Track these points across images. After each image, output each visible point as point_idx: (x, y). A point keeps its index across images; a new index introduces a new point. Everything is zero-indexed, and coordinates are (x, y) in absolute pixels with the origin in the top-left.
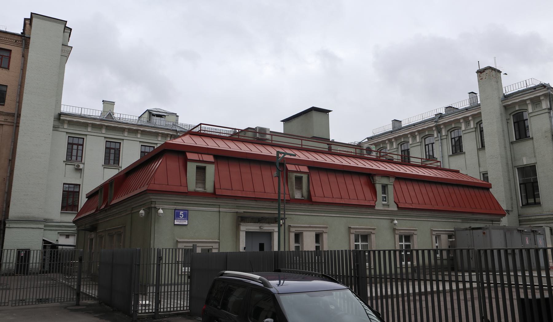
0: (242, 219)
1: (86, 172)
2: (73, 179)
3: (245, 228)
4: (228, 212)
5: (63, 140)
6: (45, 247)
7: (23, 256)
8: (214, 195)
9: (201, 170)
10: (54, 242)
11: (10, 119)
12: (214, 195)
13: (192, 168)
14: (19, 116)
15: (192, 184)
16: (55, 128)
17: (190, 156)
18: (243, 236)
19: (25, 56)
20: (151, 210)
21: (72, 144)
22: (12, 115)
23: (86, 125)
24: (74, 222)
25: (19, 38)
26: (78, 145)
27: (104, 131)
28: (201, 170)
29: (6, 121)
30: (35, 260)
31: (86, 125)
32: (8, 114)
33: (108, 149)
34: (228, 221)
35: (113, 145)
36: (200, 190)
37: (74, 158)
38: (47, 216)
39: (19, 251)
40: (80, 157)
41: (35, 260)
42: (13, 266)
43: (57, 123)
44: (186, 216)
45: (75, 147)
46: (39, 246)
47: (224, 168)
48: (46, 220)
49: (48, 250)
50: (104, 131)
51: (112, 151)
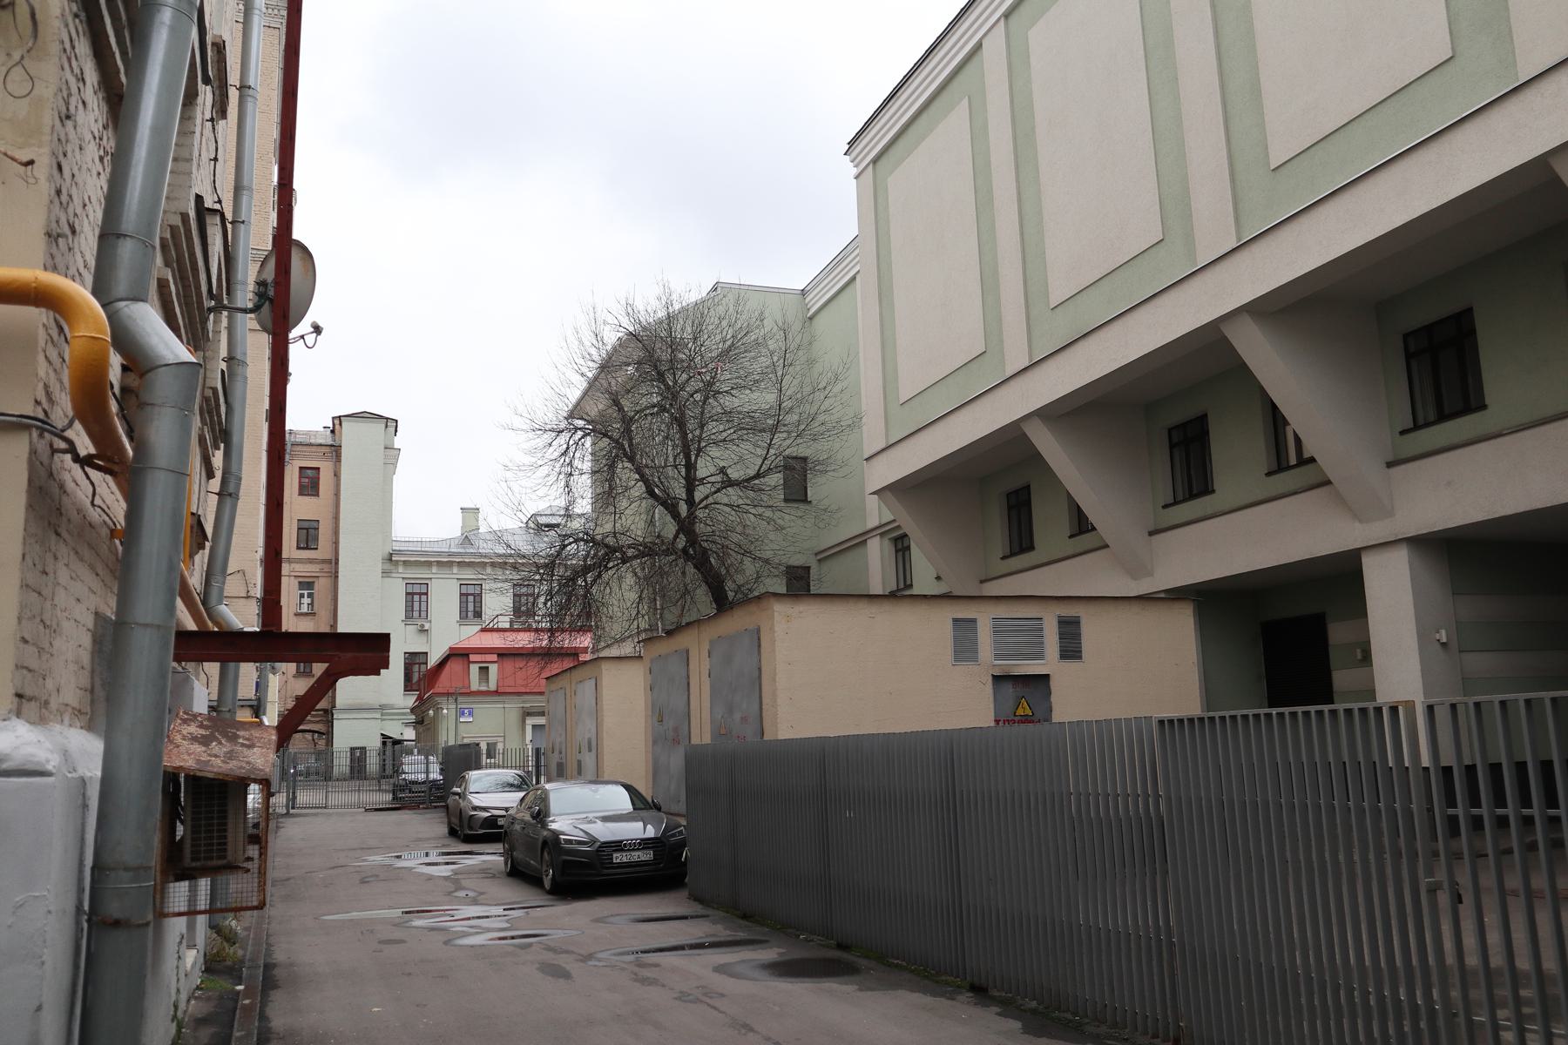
0: (527, 713)
1: (434, 633)
2: (417, 646)
3: (530, 721)
4: (513, 707)
5: (397, 590)
6: (384, 743)
7: (358, 756)
8: (496, 693)
9: (484, 671)
10: (396, 736)
11: (326, 567)
12: (496, 693)
13: (474, 669)
14: (337, 563)
15: (475, 686)
16: (386, 574)
17: (472, 658)
18: (529, 729)
19: (337, 475)
20: (438, 710)
21: (413, 594)
22: (329, 562)
23: (429, 564)
24: (413, 710)
25: (327, 450)
26: (420, 594)
27: (455, 570)
28: (484, 671)
29: (321, 570)
30: (373, 763)
31: (429, 564)
32: (324, 561)
33: (464, 596)
34: (514, 717)
35: (471, 590)
36: (484, 688)
37: (416, 614)
38: (384, 701)
39: (353, 749)
40: (424, 614)
41: (373, 763)
42: (347, 770)
43: (388, 566)
44: (471, 714)
45: (416, 598)
46: (376, 743)
47: (509, 665)
48: (382, 707)
49: (389, 745)
50: (455, 570)
51: (471, 598)
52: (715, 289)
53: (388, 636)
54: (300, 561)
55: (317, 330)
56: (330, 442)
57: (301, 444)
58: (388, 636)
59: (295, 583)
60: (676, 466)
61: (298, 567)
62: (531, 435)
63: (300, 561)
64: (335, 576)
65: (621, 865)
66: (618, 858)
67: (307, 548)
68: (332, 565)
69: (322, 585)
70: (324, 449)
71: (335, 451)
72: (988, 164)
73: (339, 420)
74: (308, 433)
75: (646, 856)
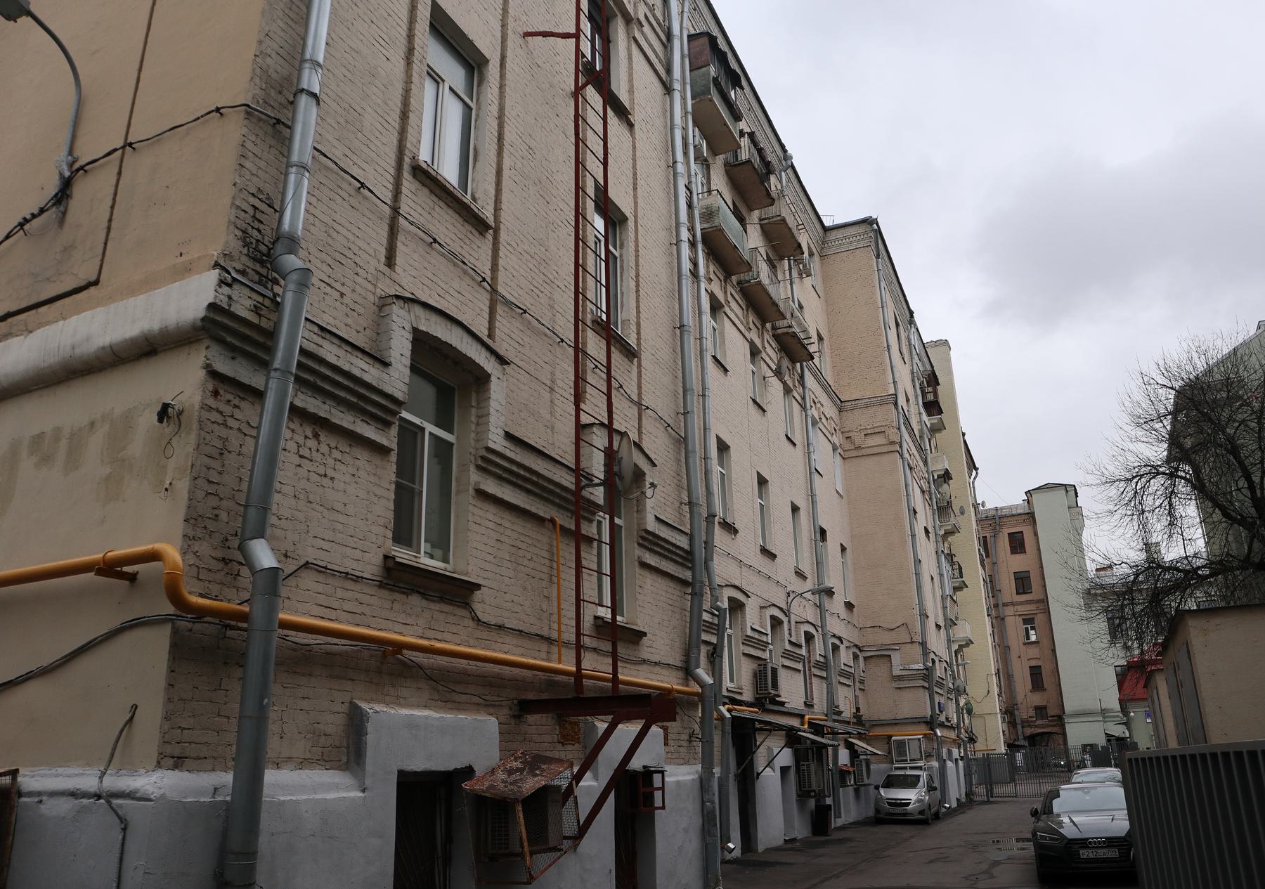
19: (1036, 534)
32: (1038, 601)
52: (1259, 328)
53: (401, 774)
54: (1021, 603)
55: (653, 485)
56: (1027, 511)
57: (1006, 516)
58: (401, 774)
59: (1020, 620)
60: (1239, 490)
61: (1019, 608)
62: (1103, 488)
63: (1021, 603)
64: (1047, 611)
65: (1088, 861)
66: (1084, 854)
67: (1024, 593)
68: (1044, 601)
69: (1039, 619)
70: (1023, 517)
71: (1030, 517)
72: (133, 342)
73: (1028, 493)
74: (1010, 507)
75: (1112, 853)
